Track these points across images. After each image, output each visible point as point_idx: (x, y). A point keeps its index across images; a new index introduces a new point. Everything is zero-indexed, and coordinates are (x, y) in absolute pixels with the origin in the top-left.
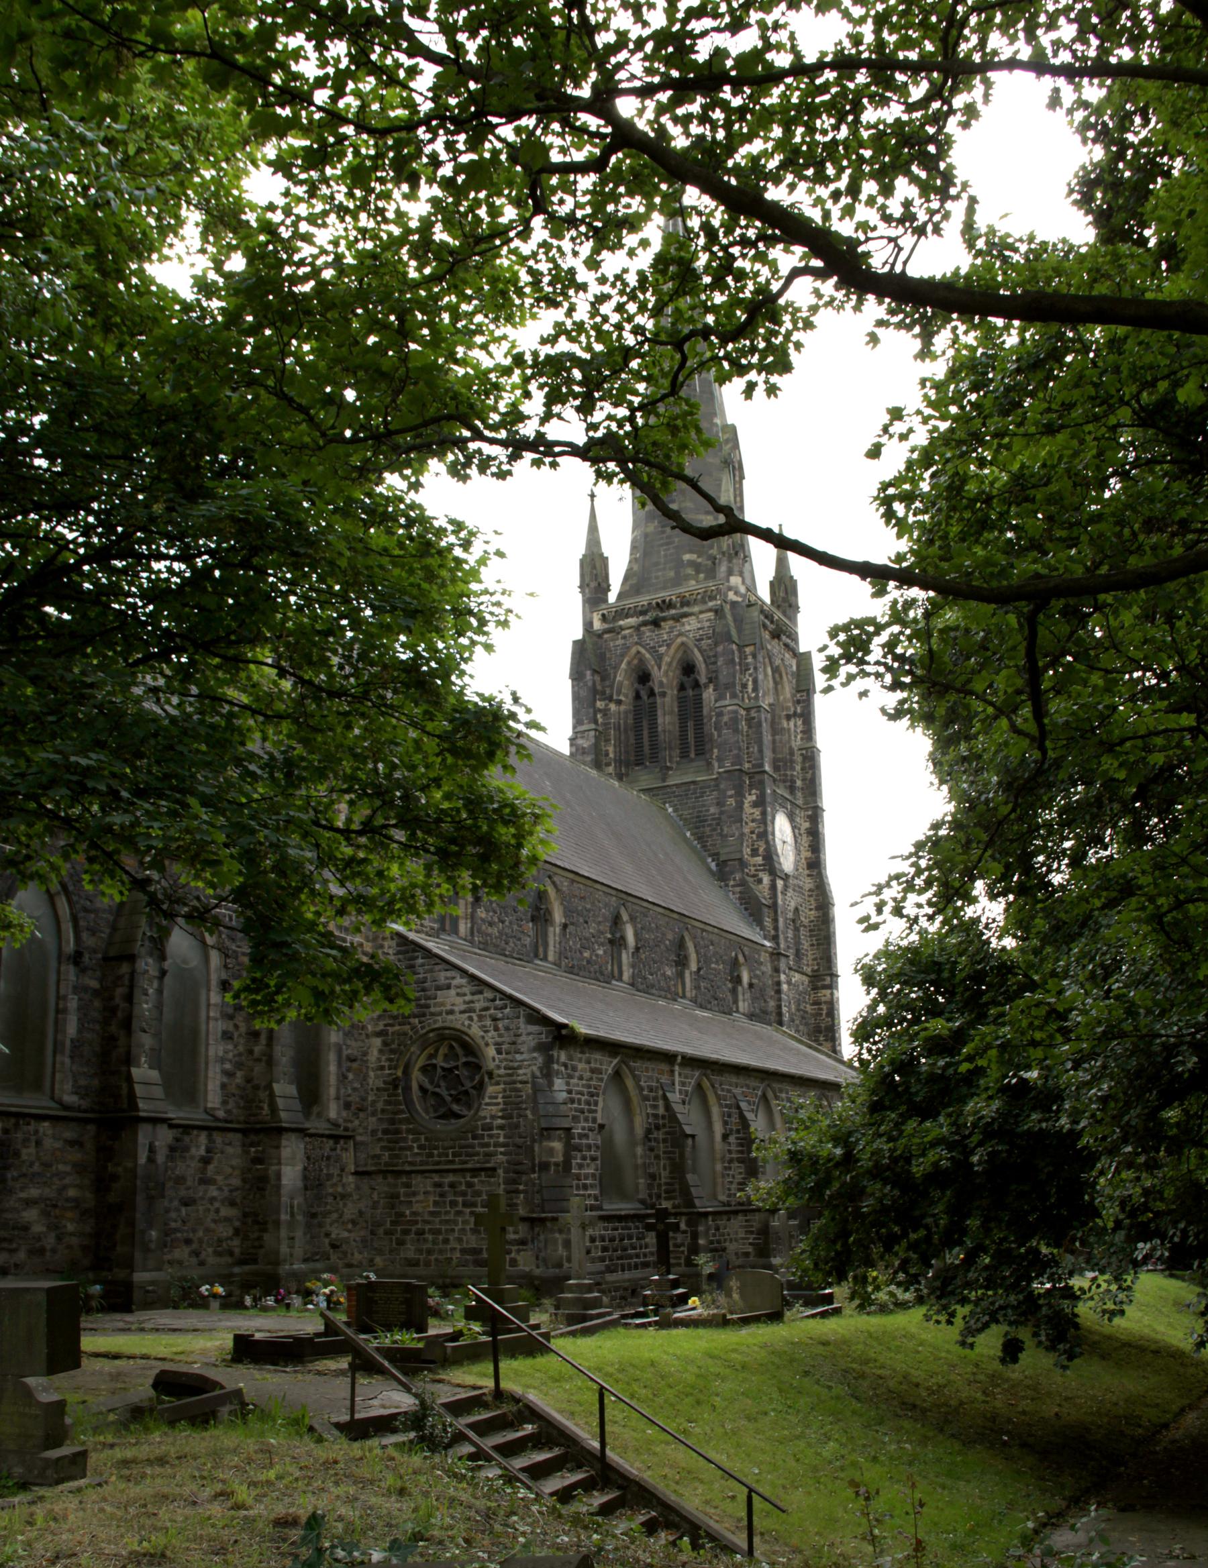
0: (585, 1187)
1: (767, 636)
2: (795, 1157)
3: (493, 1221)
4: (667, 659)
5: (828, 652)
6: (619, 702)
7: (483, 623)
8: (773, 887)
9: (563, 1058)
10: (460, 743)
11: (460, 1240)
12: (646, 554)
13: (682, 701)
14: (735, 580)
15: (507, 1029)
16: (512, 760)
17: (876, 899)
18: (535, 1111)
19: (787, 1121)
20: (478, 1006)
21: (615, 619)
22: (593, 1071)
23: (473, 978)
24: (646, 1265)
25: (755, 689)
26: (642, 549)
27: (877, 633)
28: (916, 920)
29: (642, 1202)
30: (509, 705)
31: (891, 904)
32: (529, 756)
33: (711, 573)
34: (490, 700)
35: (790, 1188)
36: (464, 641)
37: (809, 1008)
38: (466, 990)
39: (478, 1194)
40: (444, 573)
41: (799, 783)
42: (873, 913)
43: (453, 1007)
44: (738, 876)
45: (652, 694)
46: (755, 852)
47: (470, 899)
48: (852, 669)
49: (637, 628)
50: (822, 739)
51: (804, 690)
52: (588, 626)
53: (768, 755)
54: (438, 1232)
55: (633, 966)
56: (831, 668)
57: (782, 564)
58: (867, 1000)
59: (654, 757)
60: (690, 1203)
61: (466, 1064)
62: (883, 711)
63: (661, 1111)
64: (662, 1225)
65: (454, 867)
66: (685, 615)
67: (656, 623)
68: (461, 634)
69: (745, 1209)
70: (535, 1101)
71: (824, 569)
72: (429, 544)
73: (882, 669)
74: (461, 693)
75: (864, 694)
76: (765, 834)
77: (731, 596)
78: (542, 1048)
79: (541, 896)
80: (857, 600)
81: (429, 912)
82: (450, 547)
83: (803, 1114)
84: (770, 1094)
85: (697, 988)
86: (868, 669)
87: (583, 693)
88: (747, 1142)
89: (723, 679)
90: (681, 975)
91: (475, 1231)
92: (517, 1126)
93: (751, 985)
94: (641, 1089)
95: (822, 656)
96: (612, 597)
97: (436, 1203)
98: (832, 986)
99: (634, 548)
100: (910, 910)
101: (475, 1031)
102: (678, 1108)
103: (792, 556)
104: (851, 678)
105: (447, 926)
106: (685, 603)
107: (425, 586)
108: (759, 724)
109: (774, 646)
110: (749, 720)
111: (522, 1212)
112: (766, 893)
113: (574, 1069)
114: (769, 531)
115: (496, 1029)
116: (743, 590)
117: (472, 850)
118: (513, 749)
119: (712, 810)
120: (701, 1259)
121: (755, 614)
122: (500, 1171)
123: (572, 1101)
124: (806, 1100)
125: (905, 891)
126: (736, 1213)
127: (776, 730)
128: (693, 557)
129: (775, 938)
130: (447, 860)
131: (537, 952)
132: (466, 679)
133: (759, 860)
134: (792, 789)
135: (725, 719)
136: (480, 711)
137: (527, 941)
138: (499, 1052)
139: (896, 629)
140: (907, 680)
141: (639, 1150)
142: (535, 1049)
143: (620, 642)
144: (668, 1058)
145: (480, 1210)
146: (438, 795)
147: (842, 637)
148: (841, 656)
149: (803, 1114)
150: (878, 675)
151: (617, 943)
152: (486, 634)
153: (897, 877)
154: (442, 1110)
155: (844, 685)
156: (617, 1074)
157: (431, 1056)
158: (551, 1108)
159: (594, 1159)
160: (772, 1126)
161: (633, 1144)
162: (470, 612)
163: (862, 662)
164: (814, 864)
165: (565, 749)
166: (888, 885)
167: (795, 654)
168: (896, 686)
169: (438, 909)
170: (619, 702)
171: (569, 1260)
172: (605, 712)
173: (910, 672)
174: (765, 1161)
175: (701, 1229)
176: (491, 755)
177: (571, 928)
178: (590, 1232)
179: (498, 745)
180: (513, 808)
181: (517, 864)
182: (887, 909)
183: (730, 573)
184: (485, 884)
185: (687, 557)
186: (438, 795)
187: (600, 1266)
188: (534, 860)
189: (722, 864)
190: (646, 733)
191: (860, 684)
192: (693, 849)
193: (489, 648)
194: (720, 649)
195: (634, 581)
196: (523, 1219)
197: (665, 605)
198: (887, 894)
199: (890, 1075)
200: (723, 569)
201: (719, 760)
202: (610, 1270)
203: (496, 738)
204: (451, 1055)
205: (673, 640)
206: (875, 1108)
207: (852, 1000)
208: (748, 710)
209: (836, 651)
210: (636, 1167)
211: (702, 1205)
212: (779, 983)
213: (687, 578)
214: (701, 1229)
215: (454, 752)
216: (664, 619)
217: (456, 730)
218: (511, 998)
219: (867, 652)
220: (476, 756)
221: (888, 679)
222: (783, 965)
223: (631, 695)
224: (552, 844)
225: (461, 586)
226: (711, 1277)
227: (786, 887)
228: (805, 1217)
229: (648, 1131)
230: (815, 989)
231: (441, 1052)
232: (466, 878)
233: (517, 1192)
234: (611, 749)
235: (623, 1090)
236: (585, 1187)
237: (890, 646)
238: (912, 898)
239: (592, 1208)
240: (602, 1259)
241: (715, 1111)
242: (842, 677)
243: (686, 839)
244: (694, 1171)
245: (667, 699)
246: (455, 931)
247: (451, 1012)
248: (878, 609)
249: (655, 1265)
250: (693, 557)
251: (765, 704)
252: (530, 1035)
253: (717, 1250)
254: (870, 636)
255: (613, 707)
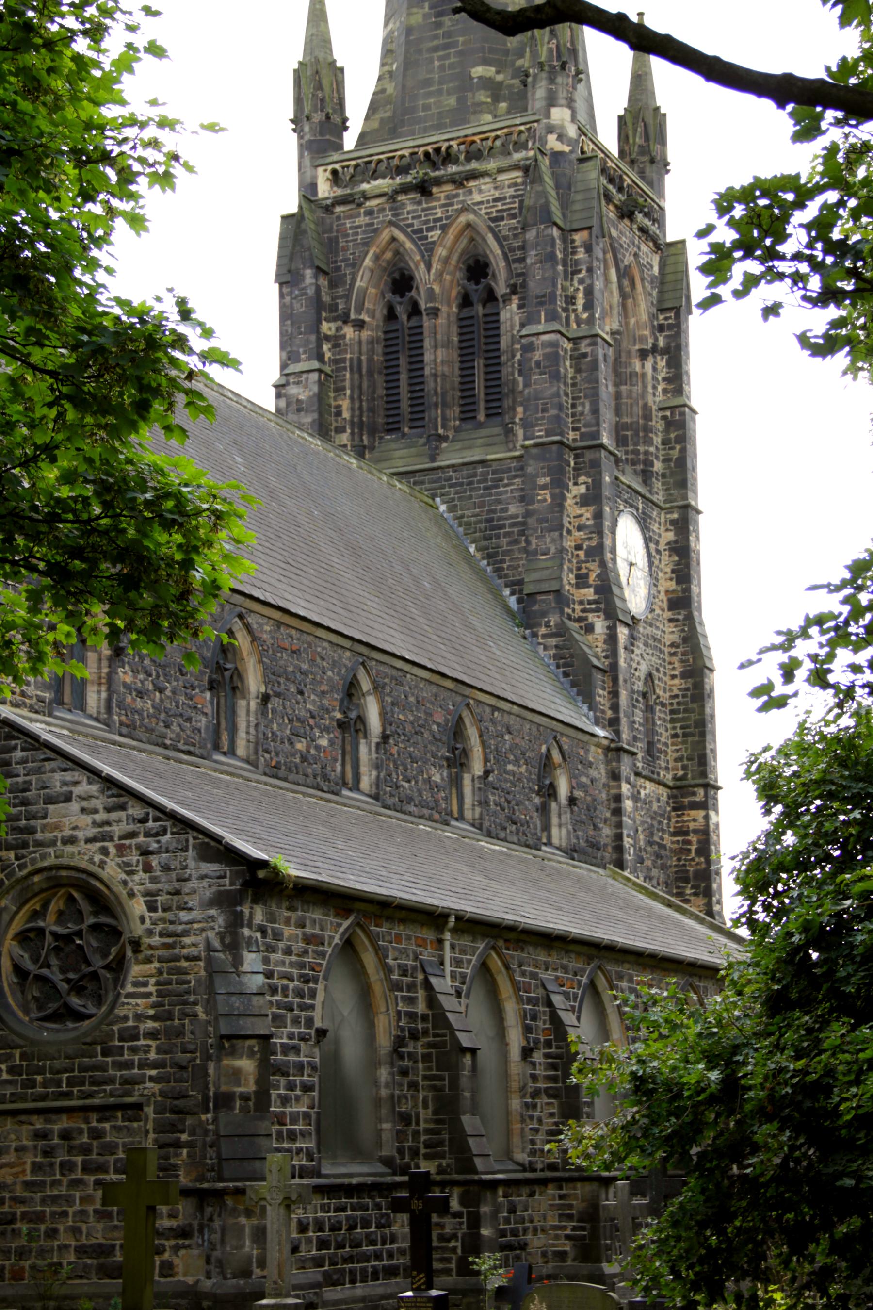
0: (292, 1136)
1: (611, 213)
2: (642, 1086)
3: (134, 1196)
4: (441, 252)
5: (714, 238)
6: (360, 325)
7: (127, 177)
8: (612, 638)
9: (259, 917)
10: (90, 387)
11: (75, 1231)
12: (408, 64)
13: (465, 324)
14: (560, 115)
15: (166, 868)
16: (181, 416)
17: (782, 657)
18: (210, 1005)
19: (631, 1027)
20: (116, 830)
21: (353, 180)
22: (308, 939)
23: (110, 782)
24: (391, 1272)
25: (589, 306)
26: (403, 55)
27: (800, 204)
28: (851, 689)
29: (387, 1162)
30: (173, 321)
31: (808, 665)
32: (208, 410)
33: (519, 101)
34: (142, 314)
35: (633, 1138)
36: (97, 209)
37: (668, 840)
38: (98, 803)
39: (110, 1149)
40: (58, 84)
41: (658, 466)
42: (777, 678)
43: (75, 828)
44: (553, 619)
45: (415, 310)
46: (582, 581)
47: (107, 652)
48: (754, 267)
49: (392, 197)
50: (700, 391)
51: (672, 311)
52: (308, 191)
53: (608, 417)
54: (39, 1217)
55: (378, 767)
56: (718, 264)
57: (640, 83)
58: (764, 824)
59: (418, 419)
60: (466, 1163)
61: (95, 928)
62: (803, 340)
63: (421, 1007)
64: (418, 1198)
65: (79, 596)
66: (474, 175)
67: (424, 189)
68: (88, 196)
69: (559, 1175)
70: (211, 991)
71: (714, 88)
72: (28, 27)
73: (804, 268)
74: (91, 297)
75: (771, 310)
76: (599, 551)
77: (553, 143)
78: (224, 901)
79: (225, 650)
80: (763, 143)
81: (35, 670)
82: (70, 36)
83: (656, 1014)
84: (602, 982)
85: (484, 803)
86: (783, 267)
87: (300, 307)
88: (563, 1059)
89: (534, 287)
90: (456, 782)
91: (102, 1215)
92: (180, 1033)
93: (572, 801)
94: (388, 970)
95: (703, 245)
96: (350, 140)
97: (37, 1168)
98: (707, 805)
99: (387, 53)
100: (839, 675)
101: (112, 871)
102: (448, 1003)
103: (658, 65)
104: (751, 282)
105: (65, 695)
106: (474, 155)
107: (25, 105)
108: (594, 366)
109: (622, 232)
110: (578, 358)
111: (184, 1179)
112: (601, 648)
113: (277, 936)
114: (622, 18)
115: (148, 869)
116: (572, 131)
117: (107, 567)
118: (181, 399)
119: (513, 509)
120: (485, 1262)
121: (591, 174)
122: (149, 1110)
123: (274, 990)
124: (663, 991)
125: (832, 644)
126: (544, 1182)
127: (621, 376)
128: (489, 71)
129: (613, 723)
130: (67, 584)
131: (218, 740)
132: (101, 276)
133: (589, 593)
134: (646, 476)
135: (538, 355)
136: (122, 334)
137: (202, 722)
138: (152, 908)
139: (832, 196)
140: (848, 286)
141: (384, 1074)
142: (213, 902)
143: (362, 220)
144: (433, 918)
145: (113, 1177)
146: (51, 474)
147: (739, 211)
148: (737, 245)
149: (656, 1014)
150: (798, 278)
151: (352, 727)
152: (132, 196)
153: (819, 621)
154: (52, 1007)
155: (738, 294)
156: (349, 946)
157: (35, 915)
158: (237, 1003)
159: (307, 1088)
160: (604, 1034)
161: (374, 1064)
162: (106, 157)
163: (772, 255)
164: (682, 602)
165: (268, 401)
166: (804, 633)
167: (658, 245)
168: (829, 295)
169: (51, 667)
170: (360, 325)
171: (262, 1263)
172: (336, 341)
173: (853, 273)
174: (593, 1091)
175: (485, 1209)
176: (142, 408)
177: (275, 703)
178: (298, 1213)
179: (156, 392)
180: (179, 498)
181: (185, 595)
182: (801, 674)
183: (551, 101)
184: (131, 626)
185: (478, 71)
186: (51, 474)
187: (314, 1274)
188: (213, 588)
189: (527, 599)
190: (403, 377)
191: (766, 293)
192: (480, 573)
193: (137, 222)
194: (531, 235)
195: (386, 113)
196: (186, 1193)
197: (439, 157)
198: (802, 649)
199: (803, 948)
200: (540, 93)
201: (527, 425)
202: (331, 1281)
203: (152, 379)
204: (71, 912)
205: (451, 219)
206: (776, 1004)
207: (740, 822)
208: (575, 341)
209: (726, 235)
210: (378, 1102)
211: (490, 1168)
212: (618, 798)
213: (479, 109)
214: (485, 1209)
215: (79, 401)
216: (438, 182)
217: (82, 365)
218: (173, 816)
219: (782, 237)
220: (118, 410)
221: (815, 283)
222: (625, 768)
223: (381, 312)
224: (242, 561)
225: (87, 110)
226: (500, 1291)
227: (632, 638)
228: (655, 1187)
229: (399, 1042)
230: (679, 808)
231: (53, 907)
232: (98, 614)
233: (178, 1145)
234: (345, 404)
235: (359, 973)
236: (292, 1136)
237: (820, 228)
238: (844, 656)
239: (303, 1172)
240: (318, 1262)
241: (511, 1008)
242: (736, 281)
243: (468, 558)
244: (475, 1110)
245: (441, 321)
246: (81, 706)
247: (71, 841)
248: (803, 161)
249: (408, 1272)
250: (489, 71)
251: (605, 328)
252: (204, 879)
253: (511, 1247)
254: (787, 210)
255: (349, 332)
